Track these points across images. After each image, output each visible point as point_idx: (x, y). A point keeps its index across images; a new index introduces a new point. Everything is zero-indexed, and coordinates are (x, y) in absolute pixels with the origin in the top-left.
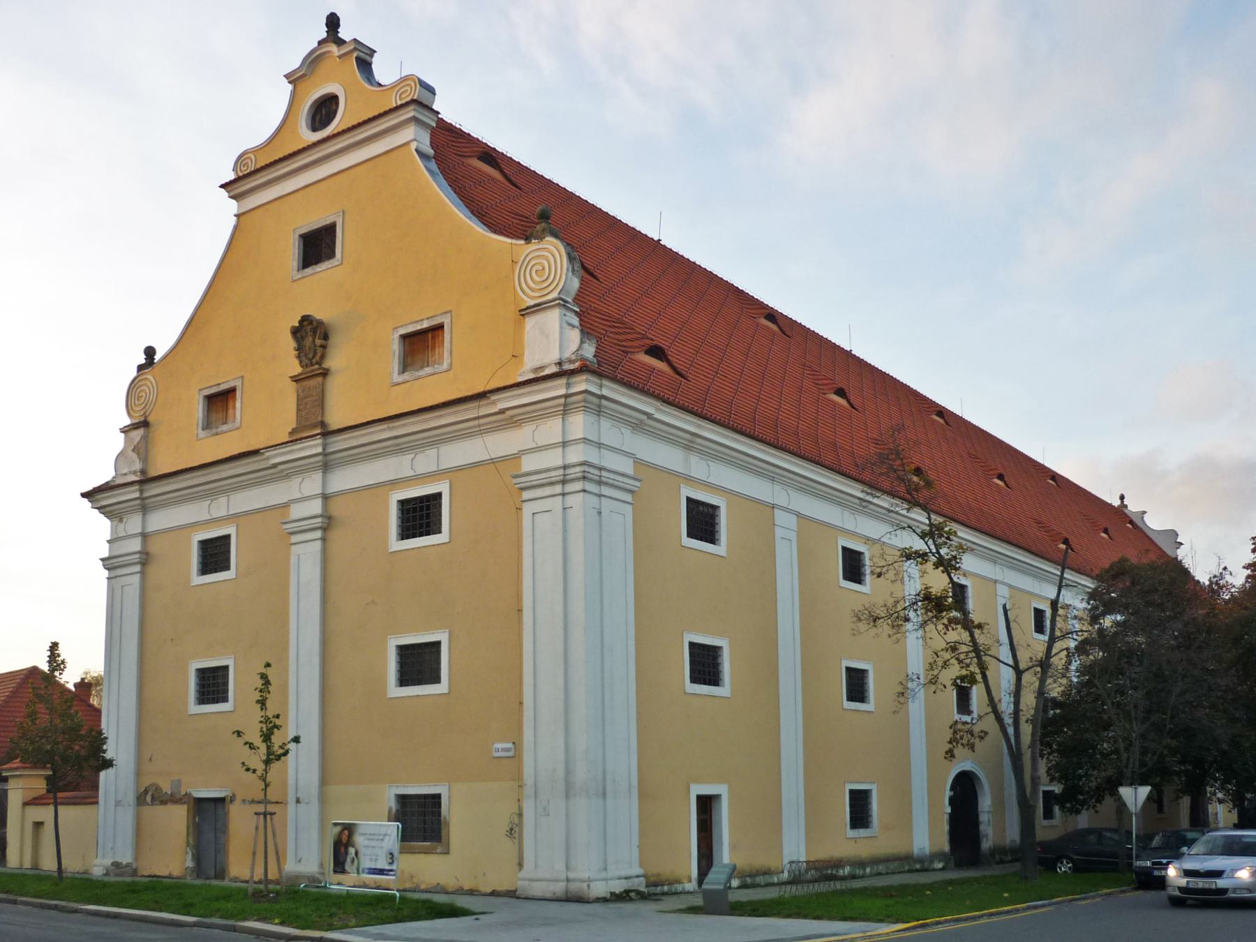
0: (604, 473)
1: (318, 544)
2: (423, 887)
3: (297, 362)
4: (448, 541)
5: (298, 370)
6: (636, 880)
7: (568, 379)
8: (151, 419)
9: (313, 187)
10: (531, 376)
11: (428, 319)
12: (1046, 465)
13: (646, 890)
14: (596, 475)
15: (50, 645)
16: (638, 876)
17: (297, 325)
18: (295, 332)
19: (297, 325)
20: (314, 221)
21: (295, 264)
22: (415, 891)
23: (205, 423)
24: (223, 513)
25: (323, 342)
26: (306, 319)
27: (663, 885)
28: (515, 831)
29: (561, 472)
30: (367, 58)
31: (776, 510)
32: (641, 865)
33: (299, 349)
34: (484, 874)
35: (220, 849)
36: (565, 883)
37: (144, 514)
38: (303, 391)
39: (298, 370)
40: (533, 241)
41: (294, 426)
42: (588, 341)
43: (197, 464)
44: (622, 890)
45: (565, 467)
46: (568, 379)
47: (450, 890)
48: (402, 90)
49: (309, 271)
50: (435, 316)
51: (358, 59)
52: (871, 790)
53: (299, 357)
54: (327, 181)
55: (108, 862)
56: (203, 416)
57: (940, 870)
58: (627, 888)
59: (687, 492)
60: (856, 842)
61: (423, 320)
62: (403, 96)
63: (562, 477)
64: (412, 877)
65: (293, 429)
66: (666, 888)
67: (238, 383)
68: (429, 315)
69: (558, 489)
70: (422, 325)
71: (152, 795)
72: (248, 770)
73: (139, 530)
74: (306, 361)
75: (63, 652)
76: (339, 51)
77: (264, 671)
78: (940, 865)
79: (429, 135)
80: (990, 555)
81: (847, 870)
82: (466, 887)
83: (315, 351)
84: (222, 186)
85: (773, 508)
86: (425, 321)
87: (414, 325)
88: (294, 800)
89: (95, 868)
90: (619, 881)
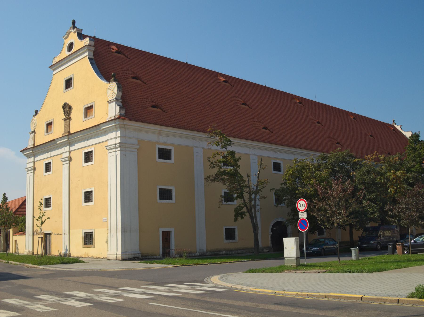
0: (126, 145)
1: (33, 173)
2: (90, 257)
3: (64, 115)
4: (94, 164)
5: (64, 117)
6: (138, 255)
7: (115, 121)
8: (35, 130)
9: (85, 58)
10: (109, 120)
11: (90, 103)
12: (356, 113)
13: (141, 257)
14: (124, 146)
15: (3, 194)
16: (138, 254)
17: (63, 105)
18: (63, 107)
19: (63, 105)
20: (67, 77)
21: (64, 88)
22: (88, 258)
23: (47, 131)
24: (50, 156)
25: (69, 110)
26: (65, 104)
27: (149, 256)
28: (107, 242)
29: (115, 145)
30: (81, 32)
31: (194, 148)
32: (140, 251)
33: (64, 111)
34: (101, 253)
35: (169, 247)
36: (116, 255)
37: (116, 132)
38: (65, 123)
39: (64, 117)
40: (111, 83)
41: (63, 132)
42: (122, 110)
43: (75, 132)
44: (132, 257)
45: (116, 144)
46: (115, 121)
47: (95, 257)
48: (86, 42)
49: (67, 90)
50: (91, 103)
51: (77, 33)
52: (171, 231)
53: (64, 114)
54: (71, 66)
55: (27, 250)
56: (46, 129)
57: (267, 252)
58: (134, 257)
59: (158, 146)
60: (228, 244)
61: (89, 104)
62: (86, 43)
63: (115, 147)
64: (87, 254)
65: (63, 133)
66: (150, 257)
67: (53, 121)
68: (90, 103)
69: (115, 150)
70: (89, 105)
71: (36, 233)
72: (38, 226)
73: (33, 161)
74: (66, 115)
75: (7, 195)
76: (73, 31)
77: (40, 201)
78: (267, 251)
79: (93, 53)
80: (287, 152)
81: (224, 252)
82: (98, 257)
83: (67, 112)
84: (49, 67)
85: (193, 147)
86: (90, 104)
87: (88, 105)
88: (64, 234)
89: (25, 252)
90: (131, 255)
